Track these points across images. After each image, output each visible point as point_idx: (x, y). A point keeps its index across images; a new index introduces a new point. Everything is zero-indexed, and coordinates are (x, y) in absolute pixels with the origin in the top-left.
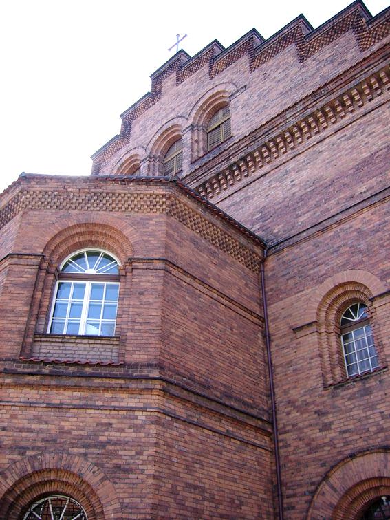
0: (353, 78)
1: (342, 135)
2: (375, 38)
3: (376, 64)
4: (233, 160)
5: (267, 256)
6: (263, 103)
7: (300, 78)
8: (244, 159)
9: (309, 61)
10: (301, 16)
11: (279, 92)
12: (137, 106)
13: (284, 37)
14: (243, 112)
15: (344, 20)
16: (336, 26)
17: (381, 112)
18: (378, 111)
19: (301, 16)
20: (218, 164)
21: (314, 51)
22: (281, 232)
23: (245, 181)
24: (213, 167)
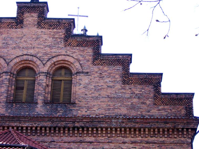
0: (149, 123)
1: (134, 146)
2: (162, 103)
3: (161, 123)
4: (77, 125)
5: (3, 133)
6: (96, 94)
7: (120, 95)
8: (83, 128)
9: (127, 87)
10: (131, 55)
11: (107, 95)
12: (52, 88)
13: (118, 59)
14: (84, 91)
15: (152, 78)
16: (147, 79)
17: (154, 147)
18: (153, 145)
19: (131, 55)
20: (68, 122)
21: (132, 84)
22: (46, 140)
23: (79, 139)
24: (64, 121)
